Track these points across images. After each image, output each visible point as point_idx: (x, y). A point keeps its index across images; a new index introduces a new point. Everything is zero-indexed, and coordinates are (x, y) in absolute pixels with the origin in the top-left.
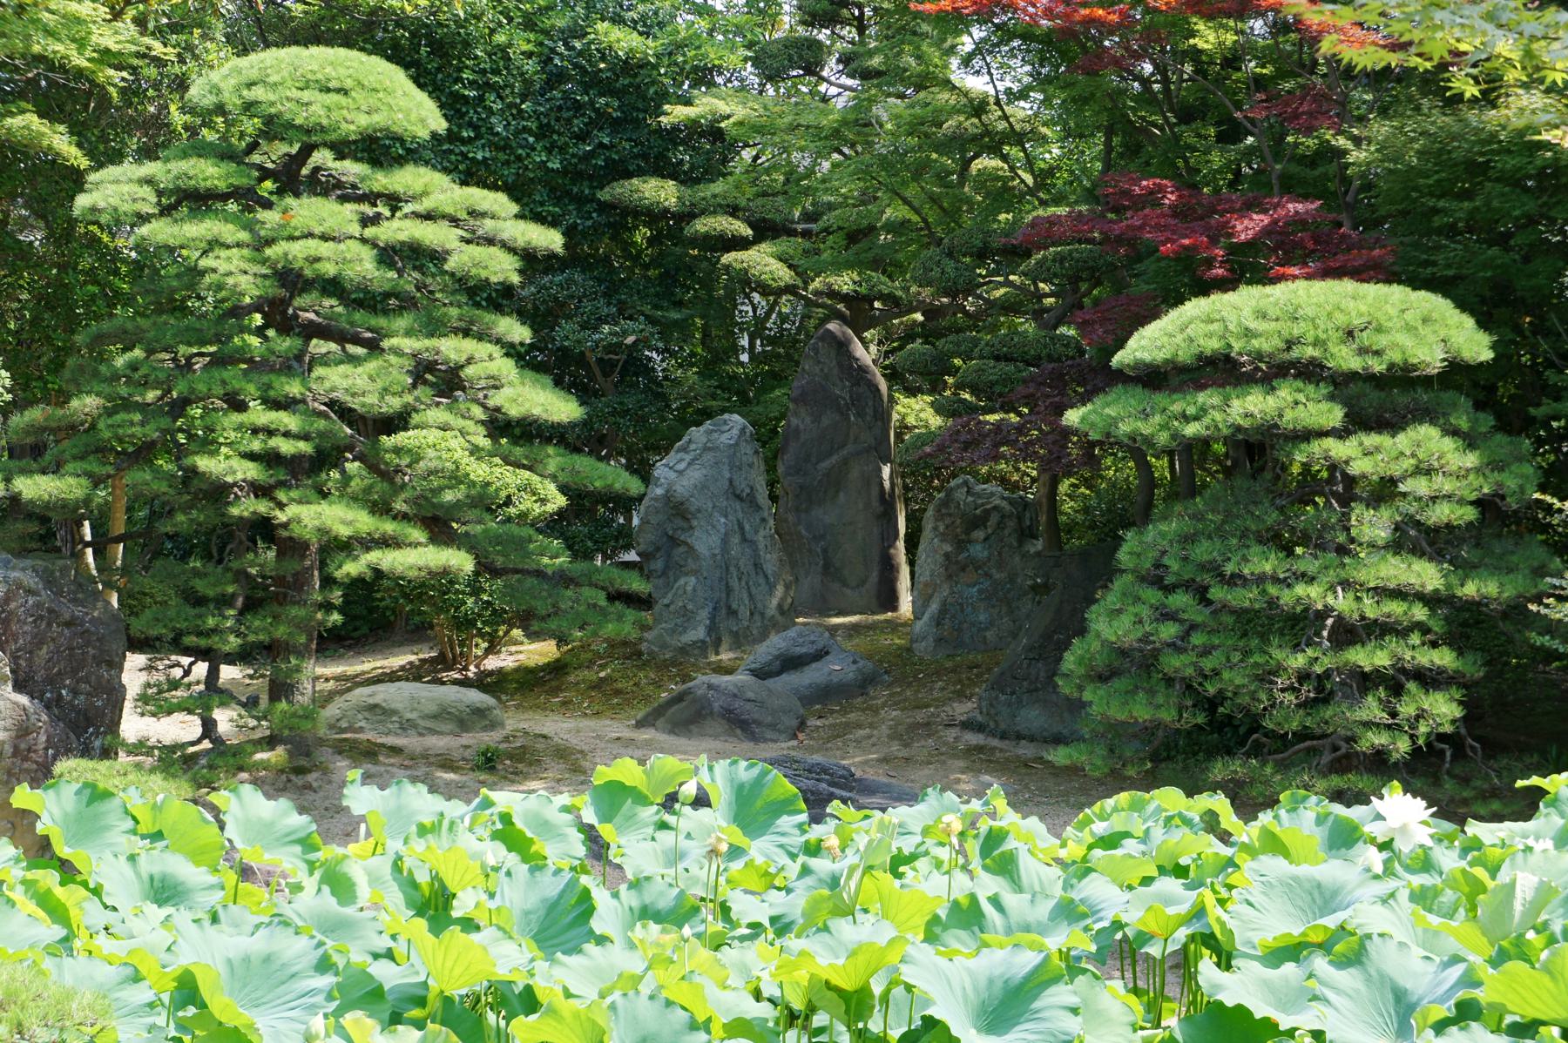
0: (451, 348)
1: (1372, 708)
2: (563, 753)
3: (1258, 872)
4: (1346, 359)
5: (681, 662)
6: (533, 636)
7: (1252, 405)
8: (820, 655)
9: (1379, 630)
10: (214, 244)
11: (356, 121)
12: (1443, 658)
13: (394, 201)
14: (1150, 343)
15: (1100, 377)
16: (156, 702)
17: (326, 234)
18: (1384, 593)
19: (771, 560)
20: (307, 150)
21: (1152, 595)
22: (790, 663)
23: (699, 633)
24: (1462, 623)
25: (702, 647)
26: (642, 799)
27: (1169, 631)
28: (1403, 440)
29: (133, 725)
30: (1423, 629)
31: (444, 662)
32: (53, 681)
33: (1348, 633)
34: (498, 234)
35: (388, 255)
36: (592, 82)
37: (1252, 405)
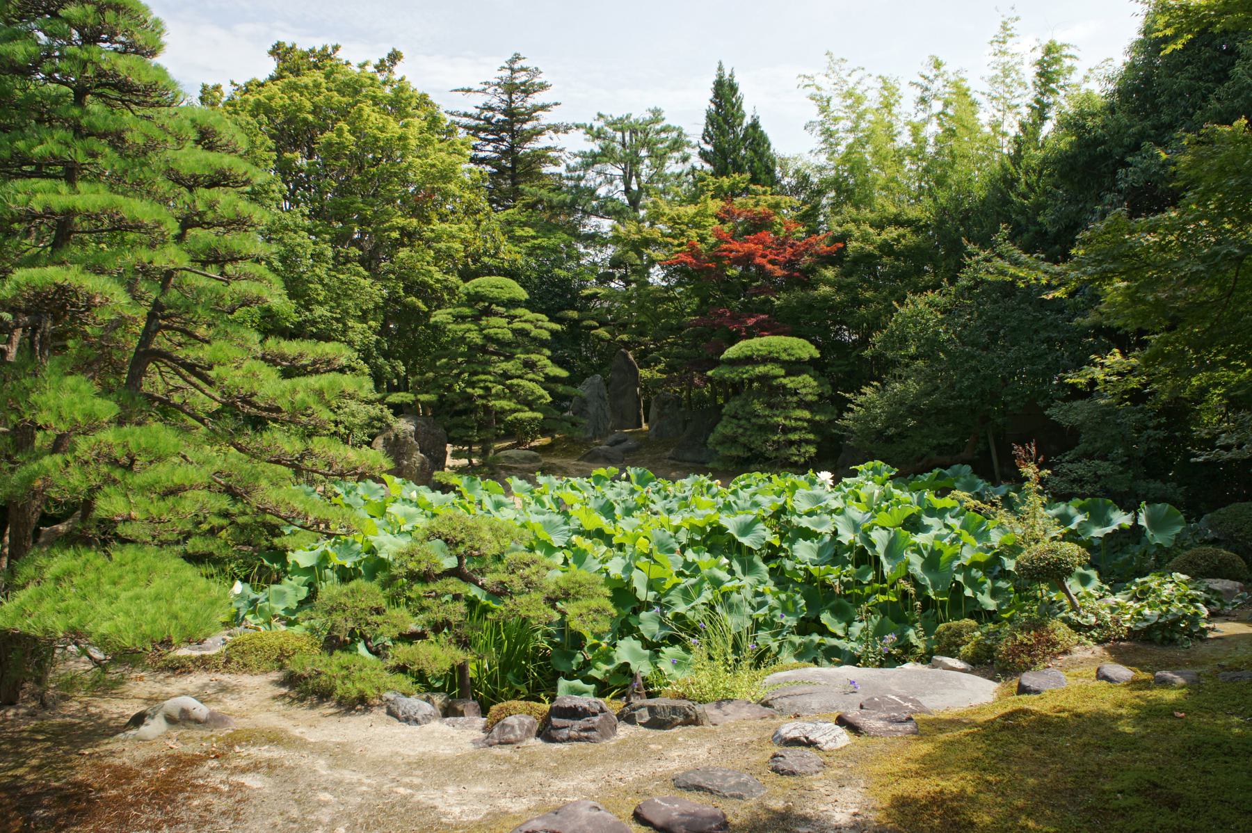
0: (534, 357)
1: (794, 450)
2: (560, 468)
3: (803, 491)
4: (784, 357)
5: (586, 442)
6: (543, 436)
7: (761, 369)
8: (625, 440)
9: (794, 430)
10: (469, 330)
11: (506, 296)
12: (811, 436)
13: (515, 317)
14: (731, 352)
15: (716, 363)
16: (456, 455)
17: (498, 326)
18: (796, 419)
19: (609, 414)
20: (490, 304)
21: (735, 421)
22: (617, 442)
23: (590, 435)
24: (814, 426)
25: (591, 439)
26: (606, 479)
27: (740, 431)
28: (800, 379)
29: (450, 461)
30: (805, 428)
31: (519, 444)
32: (429, 451)
33: (786, 430)
34: (542, 325)
35: (514, 331)
36: (554, 285)
37: (761, 369)
